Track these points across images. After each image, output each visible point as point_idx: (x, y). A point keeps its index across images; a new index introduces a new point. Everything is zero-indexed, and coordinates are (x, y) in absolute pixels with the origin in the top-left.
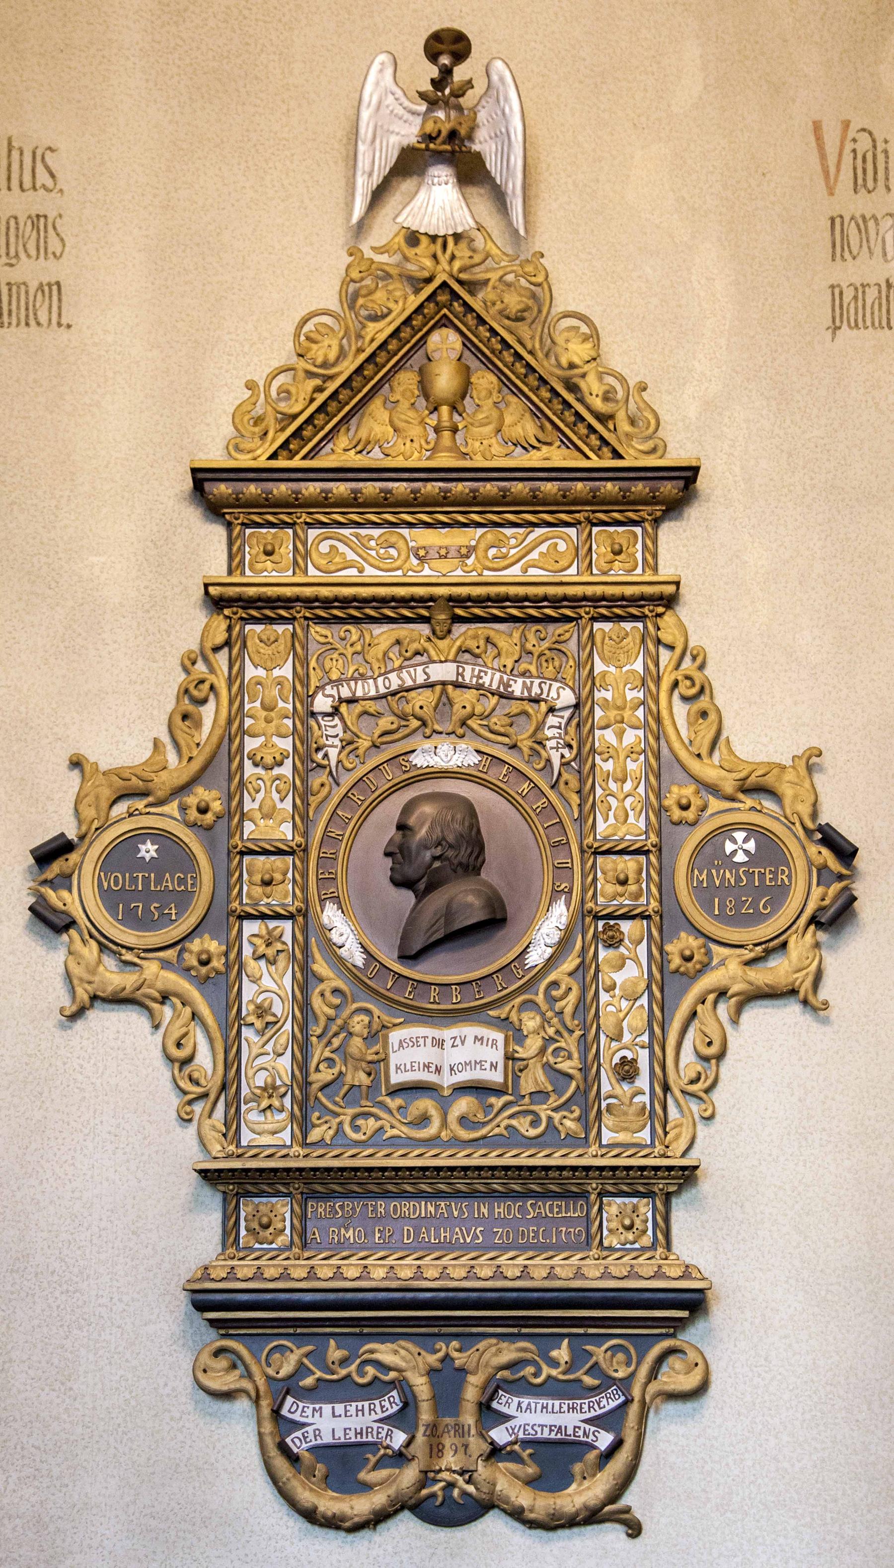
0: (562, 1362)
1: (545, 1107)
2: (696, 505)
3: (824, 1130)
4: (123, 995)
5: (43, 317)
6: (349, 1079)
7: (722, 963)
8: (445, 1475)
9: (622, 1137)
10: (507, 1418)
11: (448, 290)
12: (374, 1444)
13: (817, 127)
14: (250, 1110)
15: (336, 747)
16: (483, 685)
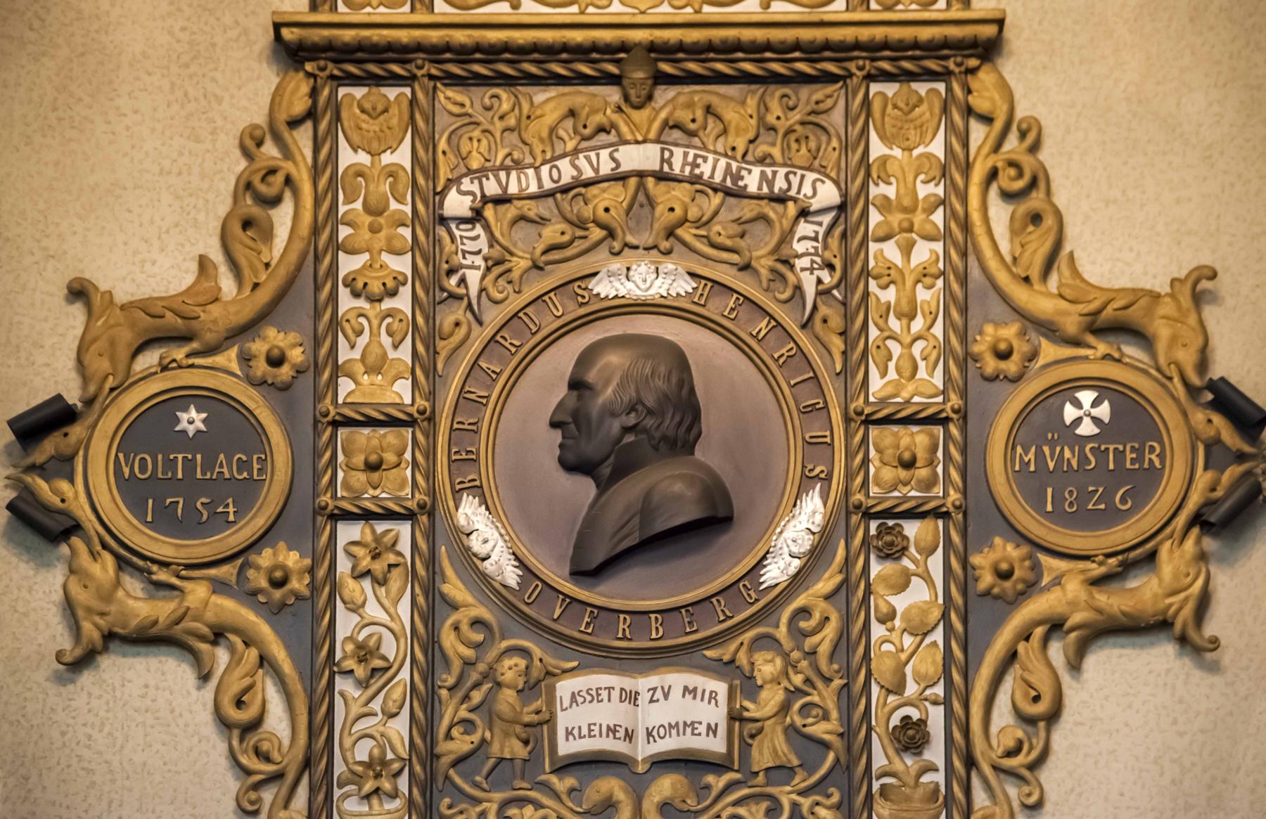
1: (788, 788)
4: (154, 631)
6: (495, 749)
7: (1057, 581)
14: (346, 796)
15: (478, 268)
16: (700, 176)
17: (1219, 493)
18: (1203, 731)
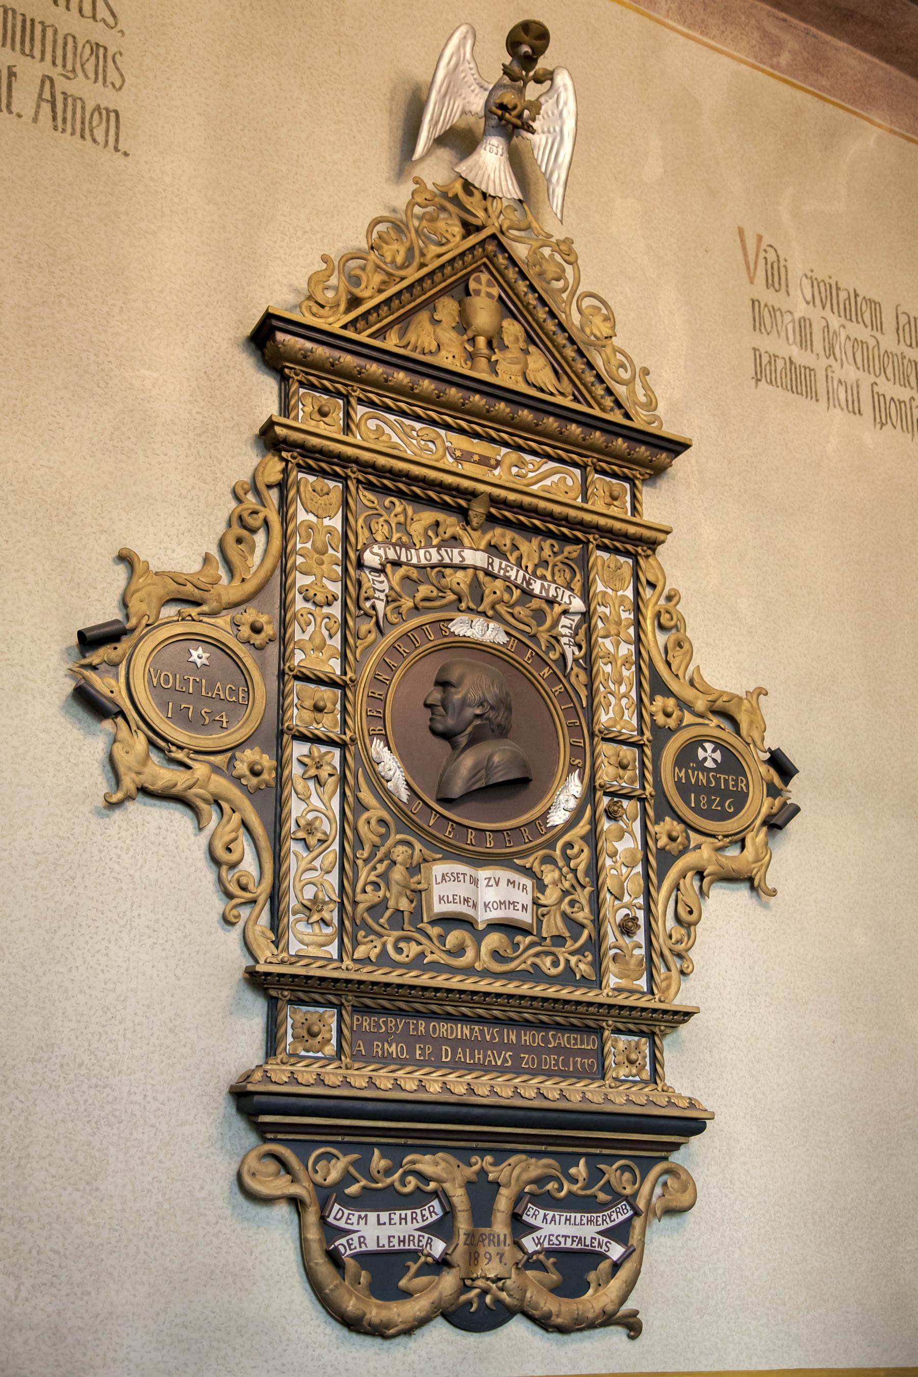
0: (581, 1179)
1: (563, 949)
2: (665, 479)
3: (767, 993)
4: (174, 791)
5: (99, 134)
6: (391, 903)
7: (698, 847)
8: (480, 1283)
9: (623, 983)
10: (534, 1229)
11: (495, 242)
12: (415, 1252)
13: (741, 232)
14: (298, 921)
15: (382, 600)
16: (509, 577)
17: (775, 810)
18: (763, 941)
